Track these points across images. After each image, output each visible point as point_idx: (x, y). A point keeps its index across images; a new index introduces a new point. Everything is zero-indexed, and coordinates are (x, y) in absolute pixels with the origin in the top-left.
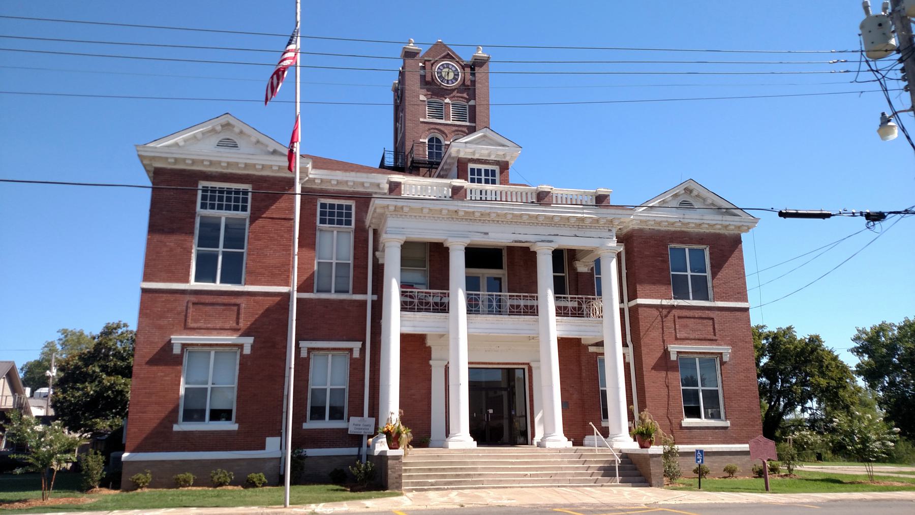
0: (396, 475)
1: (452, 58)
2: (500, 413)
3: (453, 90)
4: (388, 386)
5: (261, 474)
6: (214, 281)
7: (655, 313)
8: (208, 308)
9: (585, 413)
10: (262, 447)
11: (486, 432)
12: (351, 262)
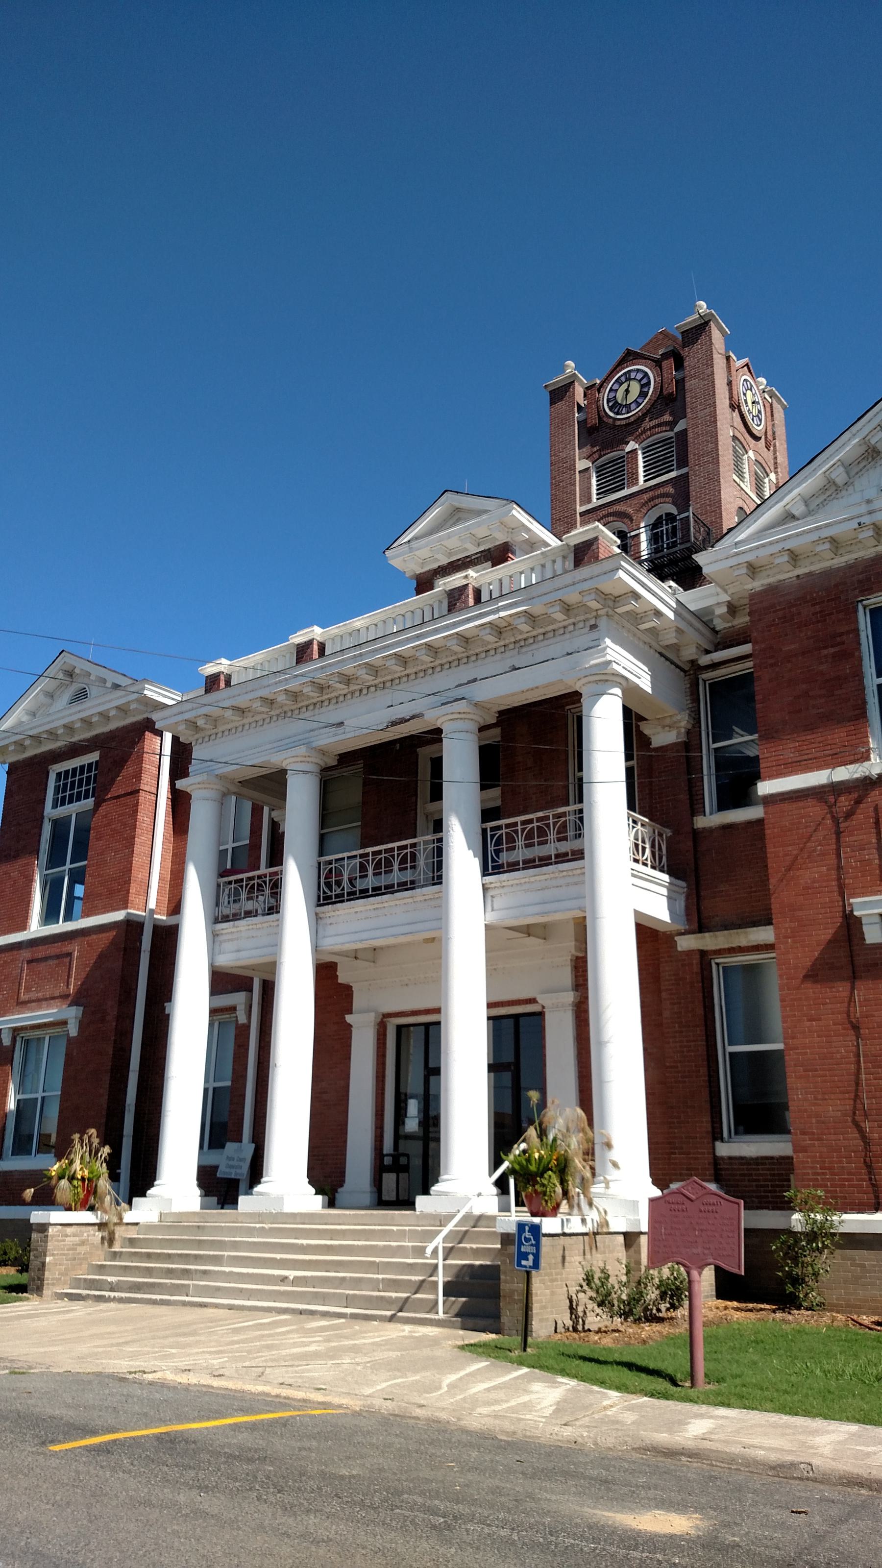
3: (640, 420)
7: (815, 810)
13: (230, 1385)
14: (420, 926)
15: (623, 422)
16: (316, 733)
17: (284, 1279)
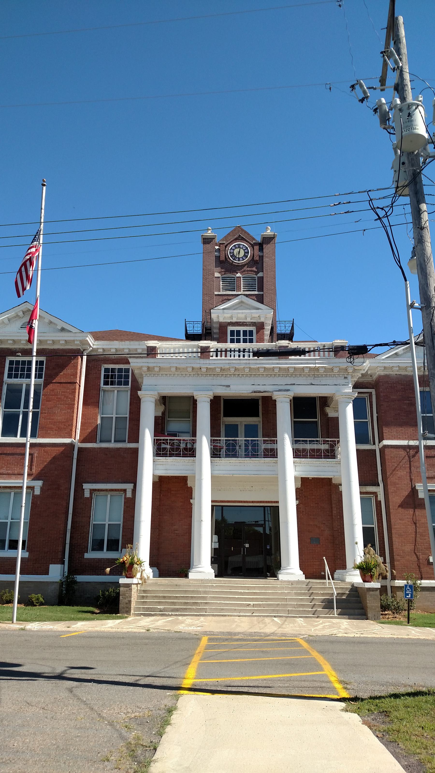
0: (126, 601)
1: (243, 239)
2: (247, 547)
3: (243, 266)
4: (287, 523)
5: (39, 595)
6: (16, 436)
7: (403, 453)
8: (9, 458)
9: (324, 548)
10: (46, 572)
11: (225, 564)
12: (128, 416)
13: (365, 636)
14: (261, 473)
15: (237, 264)
16: (215, 387)
17: (249, 605)
